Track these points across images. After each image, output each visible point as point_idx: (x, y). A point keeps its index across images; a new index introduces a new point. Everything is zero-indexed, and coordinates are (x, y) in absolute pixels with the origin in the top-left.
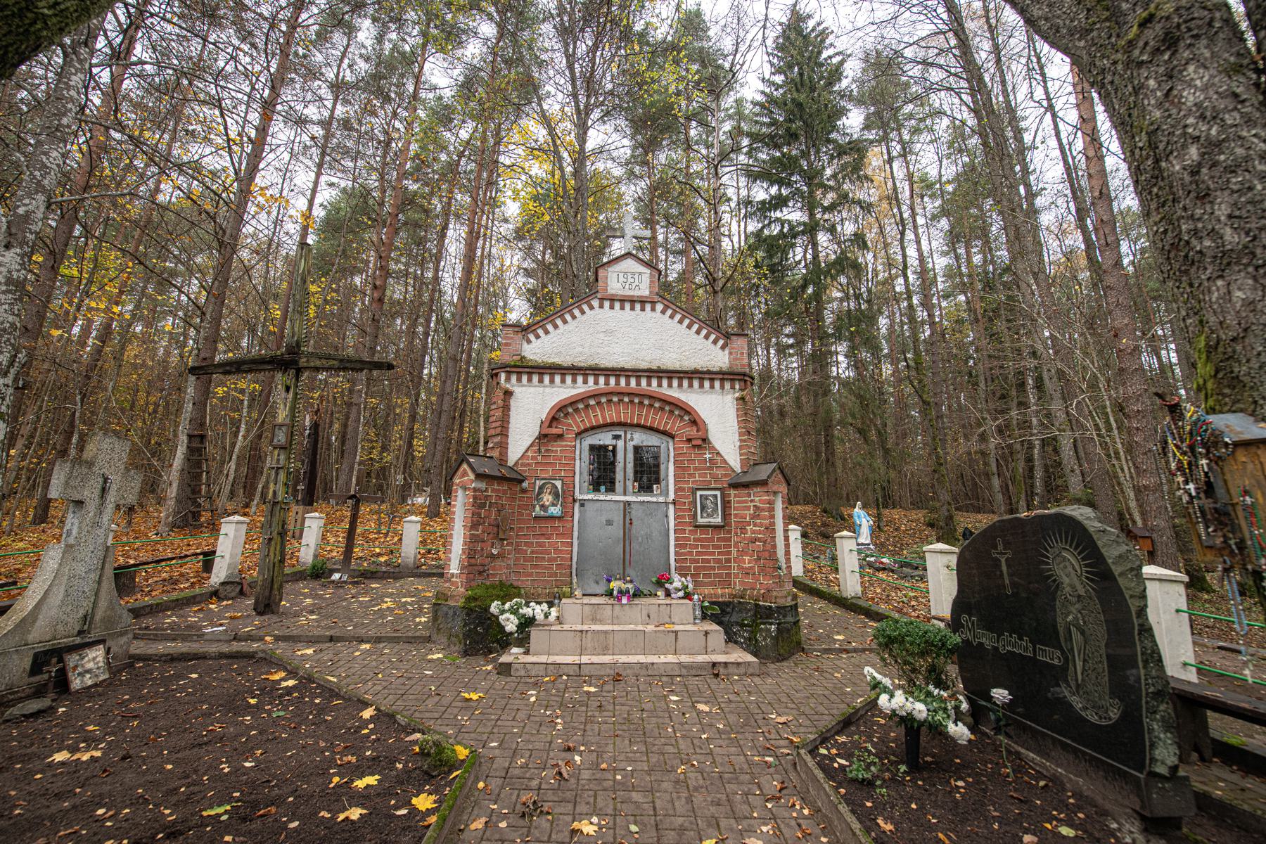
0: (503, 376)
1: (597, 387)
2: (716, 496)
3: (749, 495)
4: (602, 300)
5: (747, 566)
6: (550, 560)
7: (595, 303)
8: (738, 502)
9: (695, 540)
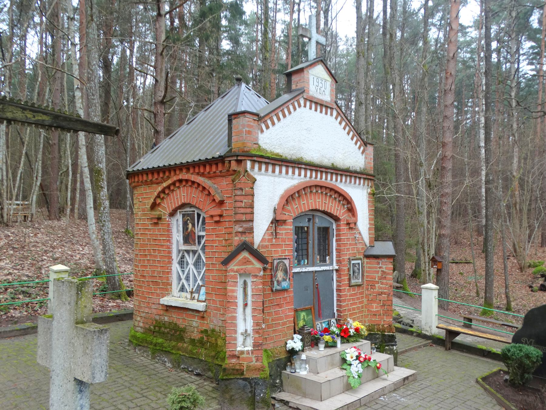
0: (249, 164)
1: (305, 180)
2: (359, 264)
3: (379, 263)
4: (306, 100)
5: (374, 310)
6: (284, 324)
7: (302, 102)
8: (370, 268)
9: (351, 295)
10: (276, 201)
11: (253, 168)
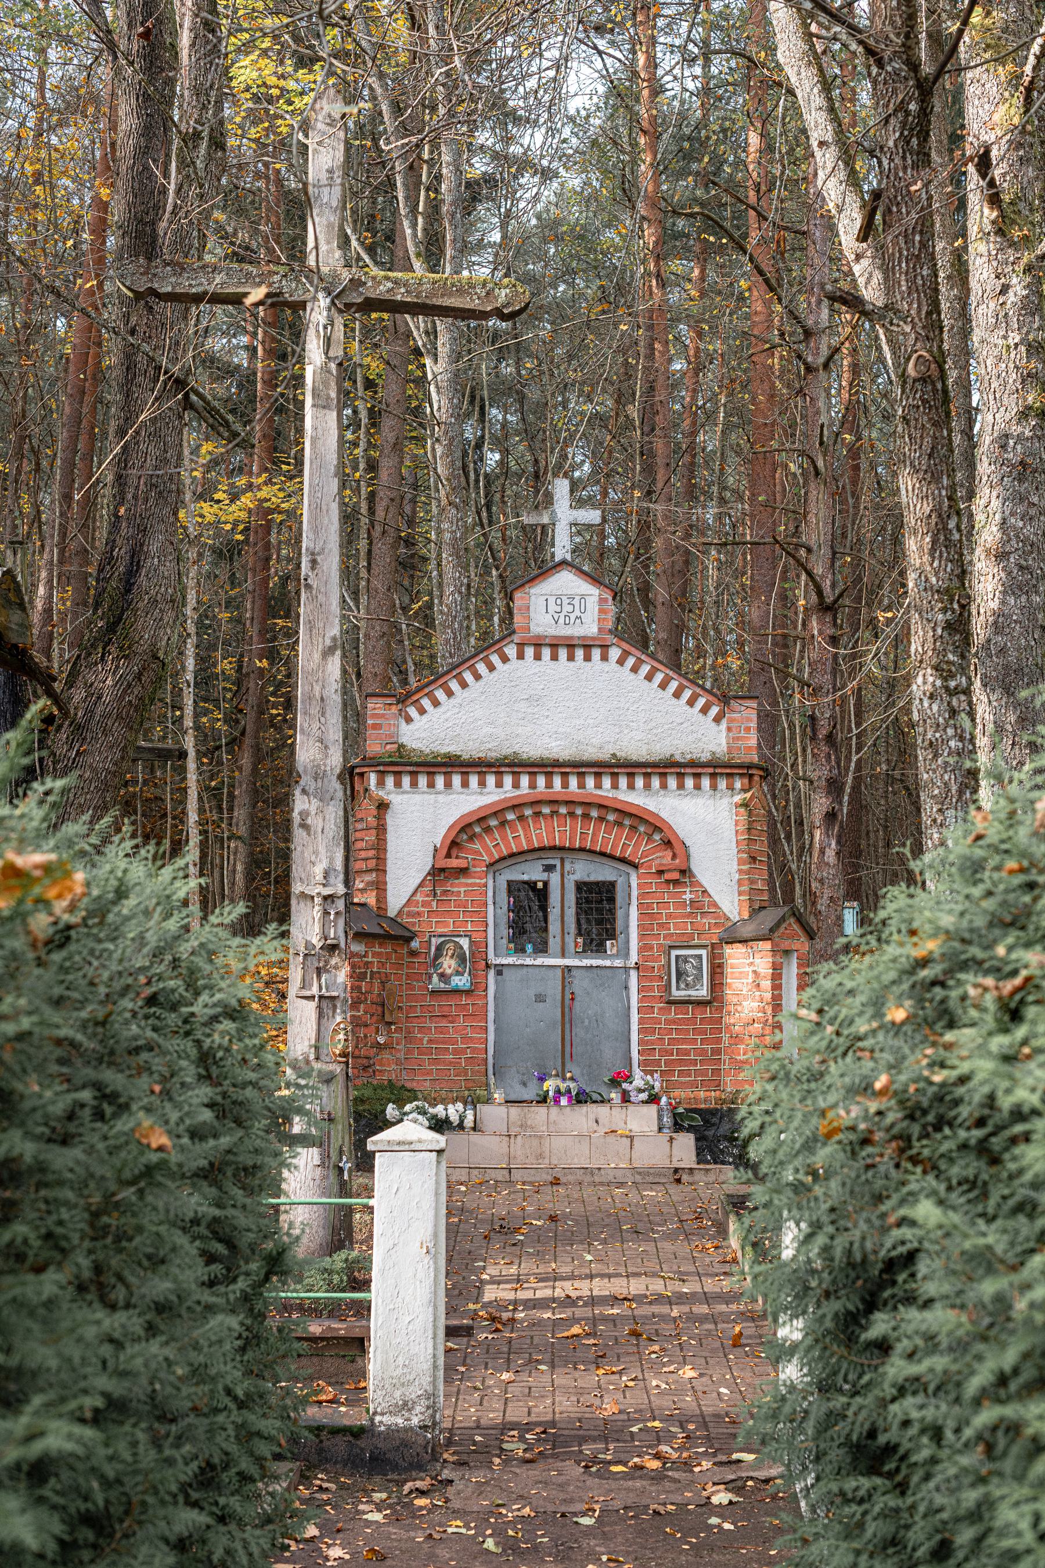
0: (373, 778)
1: (518, 793)
10: (438, 836)
11: (381, 783)
